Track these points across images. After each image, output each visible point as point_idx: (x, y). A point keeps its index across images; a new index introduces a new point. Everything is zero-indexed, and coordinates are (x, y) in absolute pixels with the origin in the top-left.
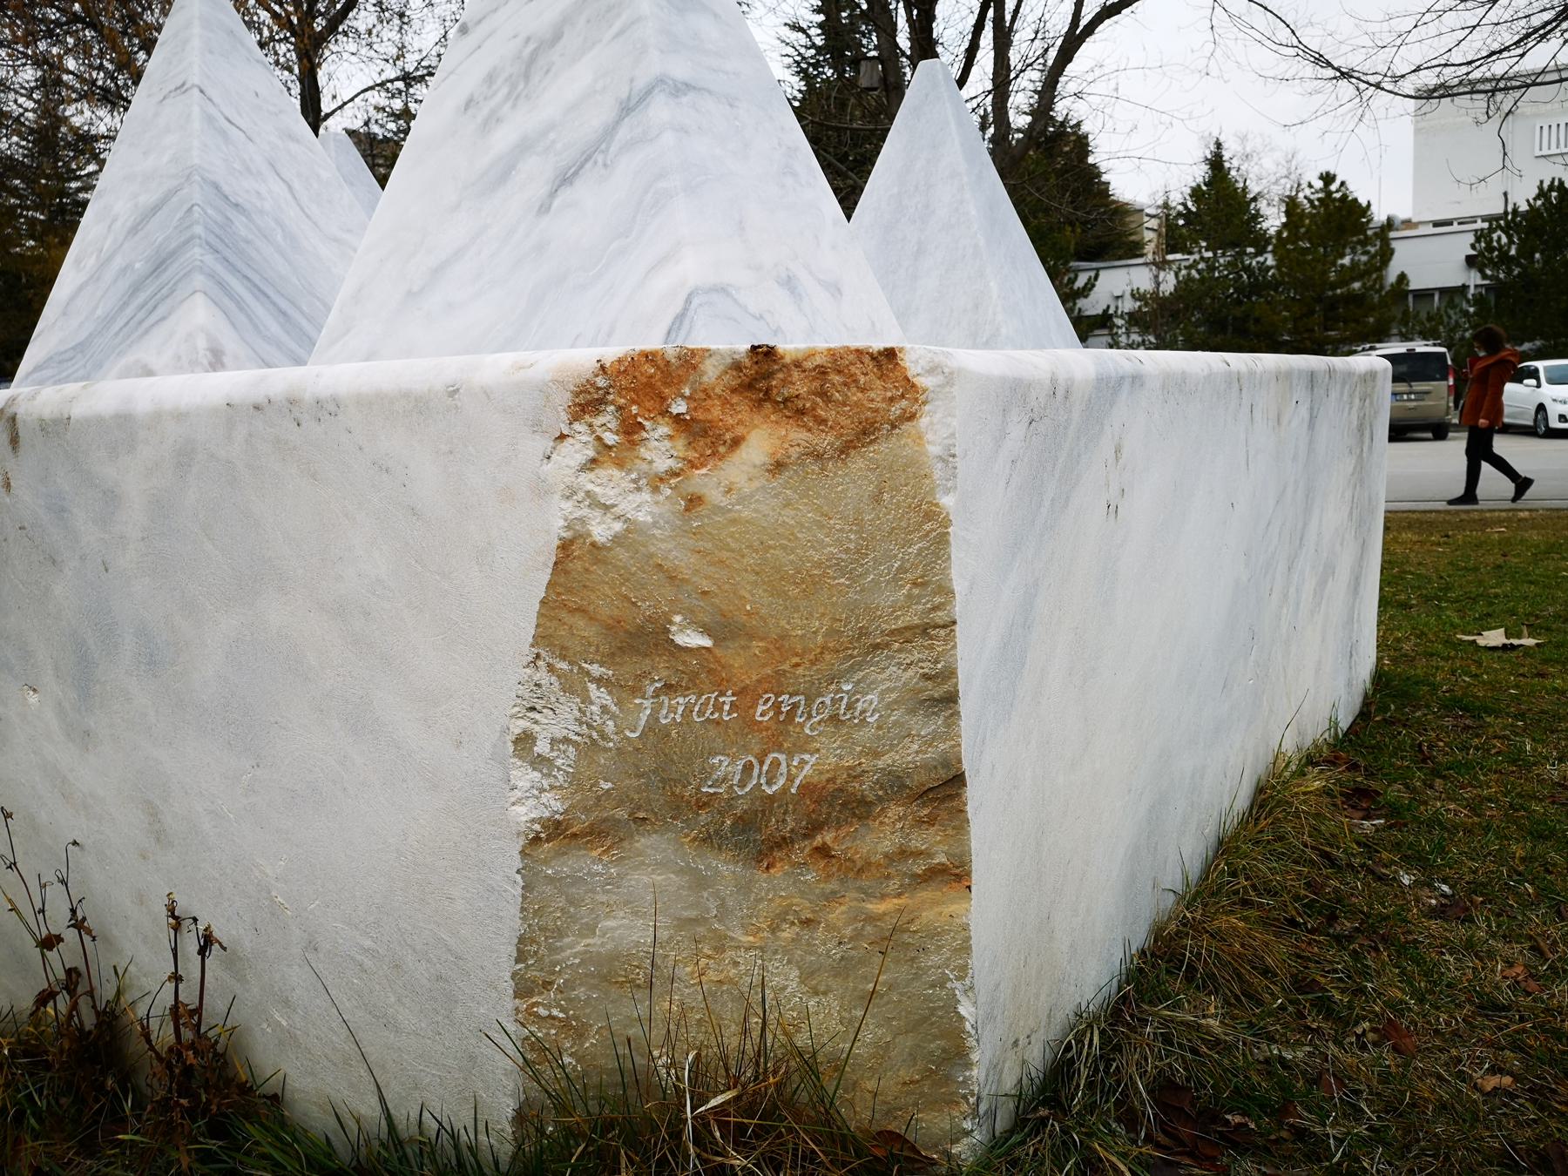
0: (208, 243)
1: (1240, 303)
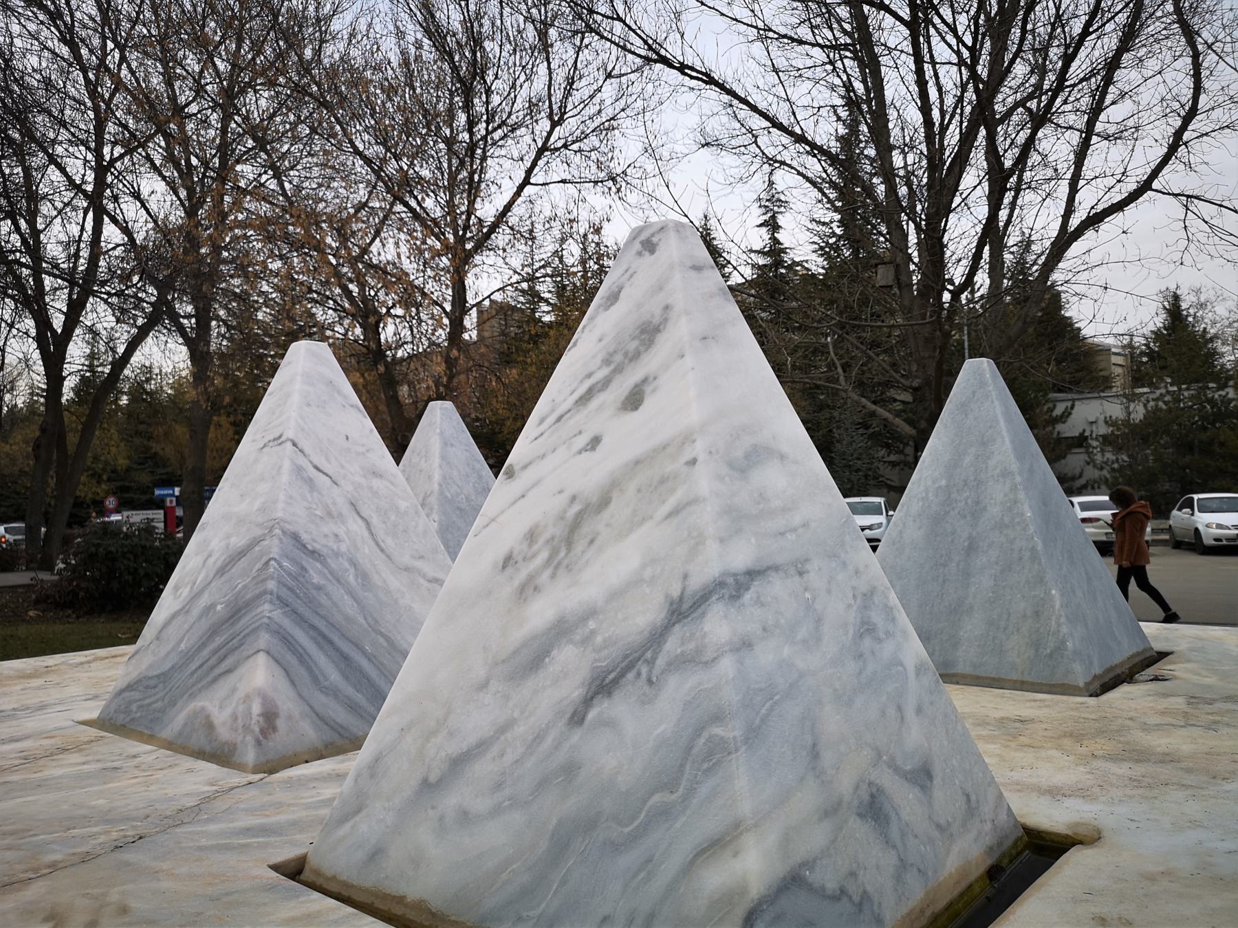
0: (279, 598)
1: (1205, 429)
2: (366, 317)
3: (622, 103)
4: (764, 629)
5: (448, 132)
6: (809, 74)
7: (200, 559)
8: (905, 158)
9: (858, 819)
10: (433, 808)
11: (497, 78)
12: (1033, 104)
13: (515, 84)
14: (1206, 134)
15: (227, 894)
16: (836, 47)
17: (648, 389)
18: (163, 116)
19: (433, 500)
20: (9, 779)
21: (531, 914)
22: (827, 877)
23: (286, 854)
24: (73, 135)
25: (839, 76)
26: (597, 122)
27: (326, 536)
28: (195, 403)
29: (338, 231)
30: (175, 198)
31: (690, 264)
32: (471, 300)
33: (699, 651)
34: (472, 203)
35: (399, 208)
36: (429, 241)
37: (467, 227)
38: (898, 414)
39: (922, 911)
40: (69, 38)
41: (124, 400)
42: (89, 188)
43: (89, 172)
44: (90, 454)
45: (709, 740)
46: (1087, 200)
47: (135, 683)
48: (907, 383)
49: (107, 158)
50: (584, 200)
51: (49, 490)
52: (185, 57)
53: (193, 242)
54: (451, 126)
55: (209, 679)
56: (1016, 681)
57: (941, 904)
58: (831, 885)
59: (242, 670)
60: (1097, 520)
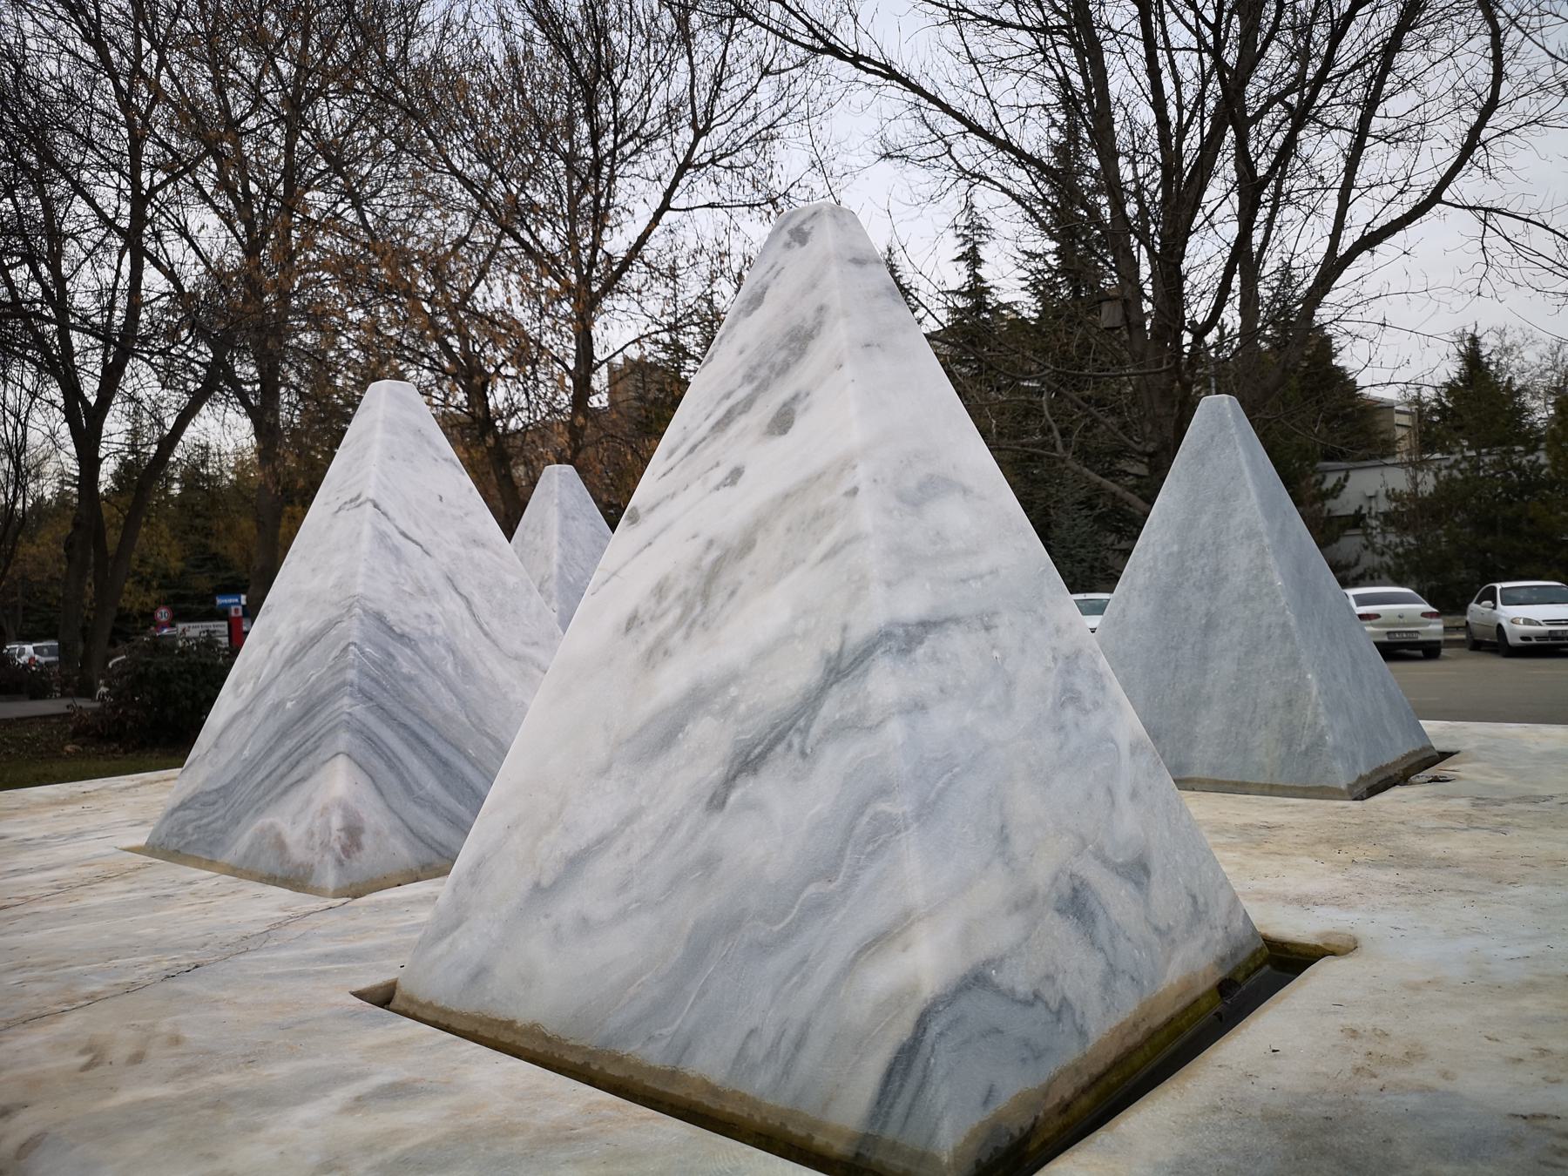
0: (361, 690)
2: (469, 378)
3: (783, 106)
4: (942, 691)
5: (567, 146)
6: (1014, 65)
7: (264, 649)
8: (1135, 169)
9: (1056, 914)
10: (547, 916)
11: (626, 76)
12: (1293, 99)
13: (649, 86)
14: (1509, 132)
15: (300, 1022)
16: (1045, 29)
17: (799, 408)
18: (213, 134)
19: (552, 585)
20: (38, 909)
21: (664, 1031)
22: (1019, 979)
23: (373, 979)
24: (102, 156)
25: (1052, 68)
26: (752, 129)
27: (417, 617)
28: (263, 487)
29: (434, 271)
30: (229, 233)
31: (849, 256)
32: (599, 355)
33: (861, 715)
34: (597, 234)
35: (508, 242)
36: (546, 283)
37: (592, 264)
38: (1132, 489)
39: (1136, 1025)
40: (94, 36)
41: (176, 489)
42: (125, 224)
43: (123, 204)
44: (134, 556)
45: (874, 818)
46: (1361, 216)
47: (192, 799)
48: (1139, 448)
49: (146, 186)
50: (737, 229)
51: (87, 601)
52: (239, 58)
53: (254, 289)
54: (570, 139)
55: (279, 790)
56: (1264, 785)
57: (1160, 1018)
58: (1023, 989)
59: (317, 778)
60: (1377, 616)
